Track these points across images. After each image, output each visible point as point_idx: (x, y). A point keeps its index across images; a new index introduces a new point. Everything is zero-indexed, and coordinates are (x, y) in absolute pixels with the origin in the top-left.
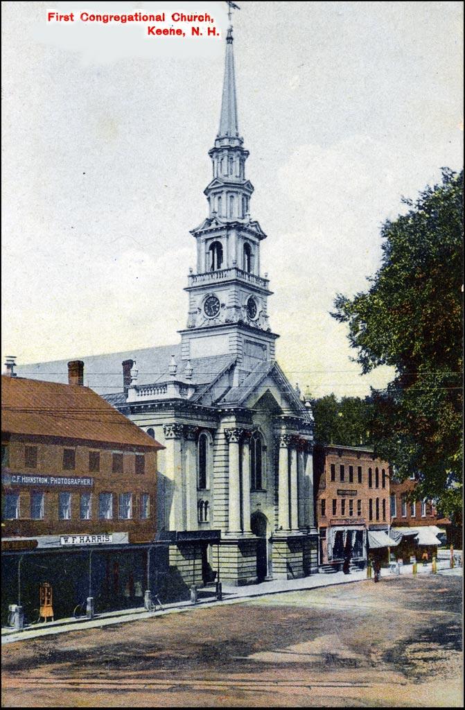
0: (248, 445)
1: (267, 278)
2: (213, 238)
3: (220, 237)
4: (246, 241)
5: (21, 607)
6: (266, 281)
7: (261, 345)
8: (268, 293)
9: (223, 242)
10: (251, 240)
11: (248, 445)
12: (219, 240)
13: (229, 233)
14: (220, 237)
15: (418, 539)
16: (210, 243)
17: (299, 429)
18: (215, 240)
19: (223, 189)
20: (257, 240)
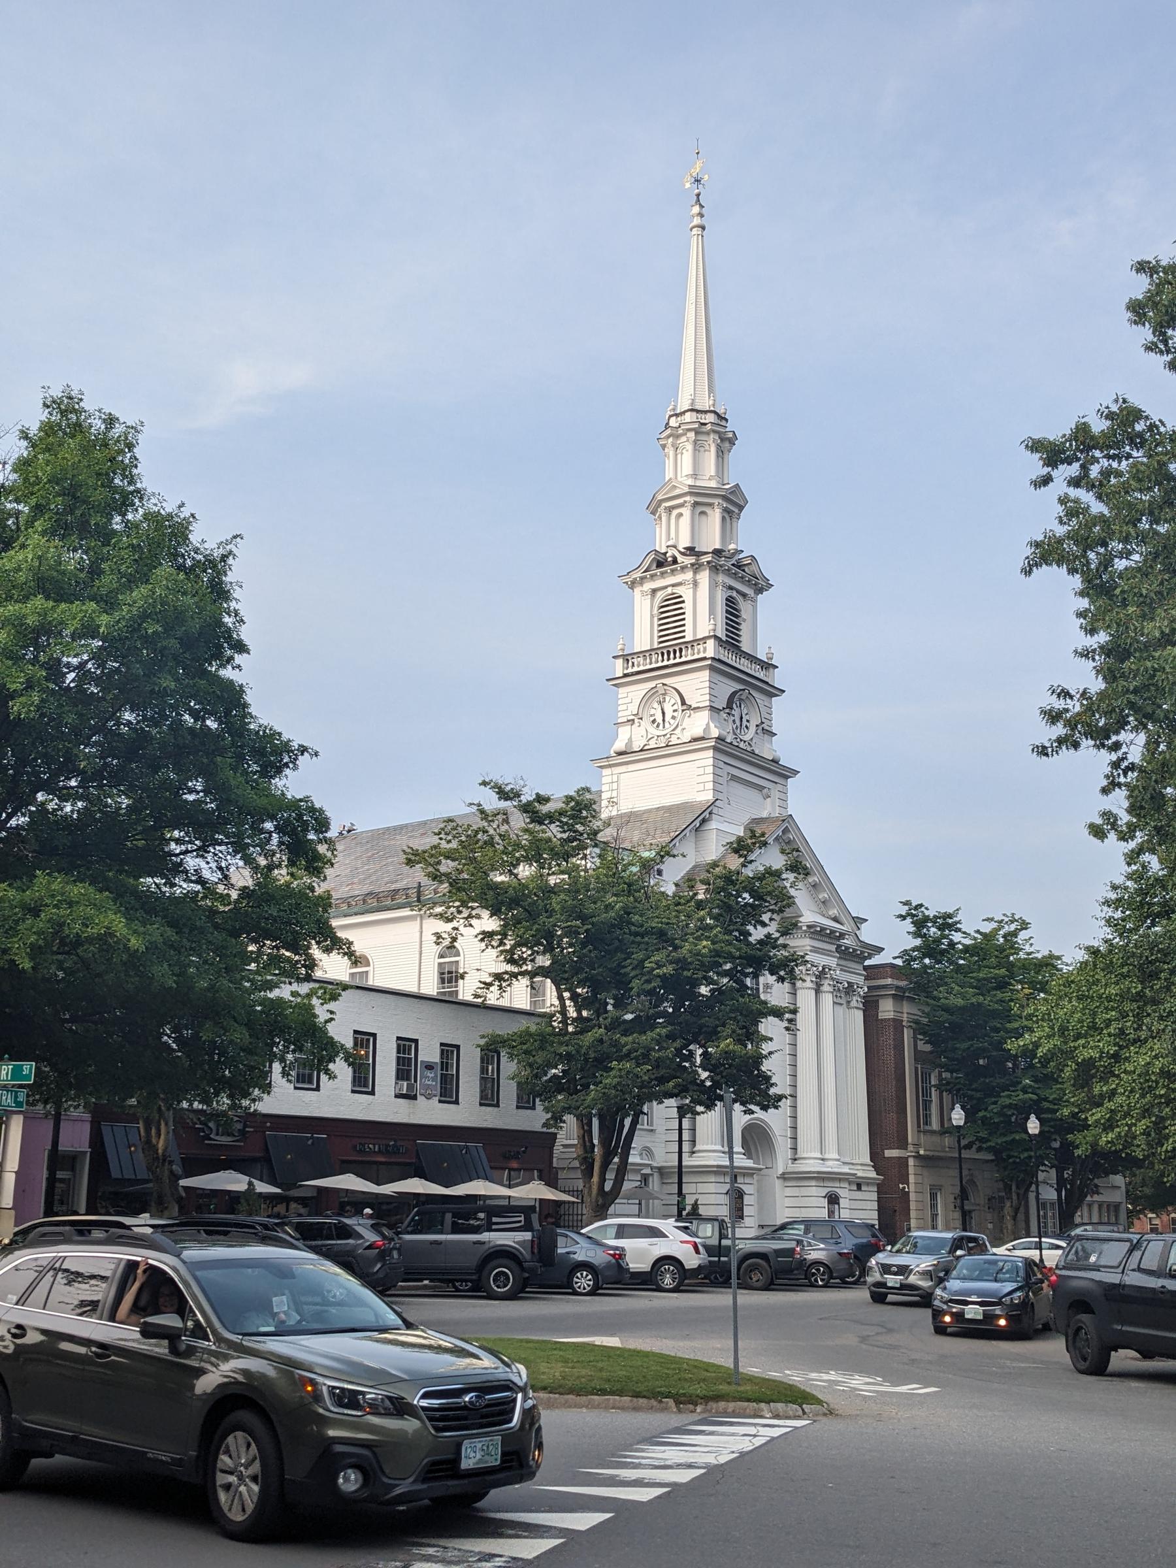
0: (21, 1117)
1: (773, 662)
2: (666, 587)
3: (679, 584)
4: (730, 593)
5: (1012, 1045)
6: (767, 666)
7: (760, 788)
8: (773, 692)
9: (686, 592)
10: (738, 592)
11: (21, 1117)
12: (679, 590)
13: (698, 577)
14: (679, 584)
15: (533, 1108)
16: (660, 595)
17: (135, 626)
18: (669, 590)
19: (688, 498)
20: (749, 591)
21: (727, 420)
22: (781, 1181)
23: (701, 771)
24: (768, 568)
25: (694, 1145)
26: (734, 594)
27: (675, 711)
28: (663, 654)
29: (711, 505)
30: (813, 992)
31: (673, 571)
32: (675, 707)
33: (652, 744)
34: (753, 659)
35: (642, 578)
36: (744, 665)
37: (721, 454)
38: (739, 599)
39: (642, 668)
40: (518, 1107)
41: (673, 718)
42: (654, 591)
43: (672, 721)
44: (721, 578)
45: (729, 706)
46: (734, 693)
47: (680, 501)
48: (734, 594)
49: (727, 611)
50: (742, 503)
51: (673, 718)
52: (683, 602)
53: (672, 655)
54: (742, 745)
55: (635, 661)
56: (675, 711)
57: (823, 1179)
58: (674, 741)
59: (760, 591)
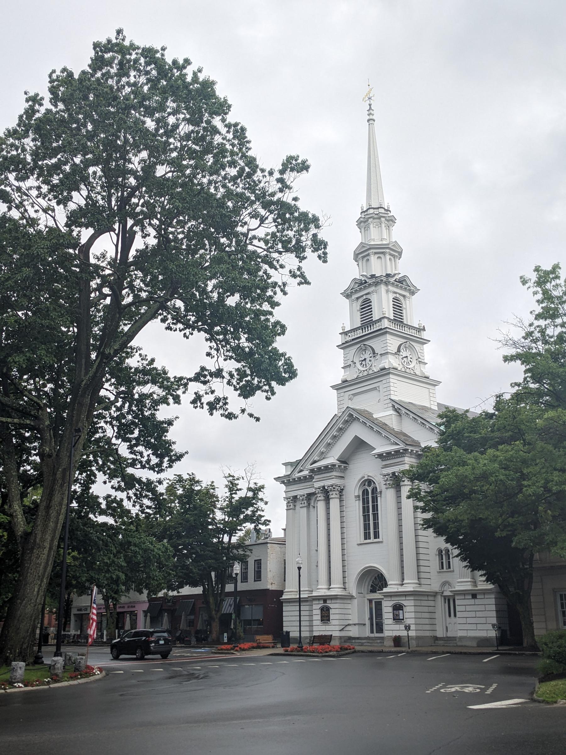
2: (362, 296)
10: (400, 294)
16: (361, 300)
18: (364, 297)
20: (407, 294)
21: (390, 211)
22: (353, 596)
23: (395, 385)
24: (414, 280)
25: (403, 579)
26: (398, 296)
27: (371, 357)
28: (362, 329)
29: (368, 255)
30: (338, 500)
31: (365, 287)
32: (371, 355)
33: (361, 375)
34: (411, 327)
35: (351, 293)
36: (407, 331)
37: (388, 227)
38: (401, 298)
39: (353, 337)
40: (261, 560)
41: (370, 361)
42: (358, 298)
43: (370, 363)
44: (391, 288)
45: (399, 350)
46: (401, 345)
47: (367, 253)
48: (398, 296)
49: (393, 305)
50: (400, 251)
51: (370, 361)
52: (371, 302)
53: (367, 329)
54: (408, 371)
55: (406, 329)
56: (371, 357)
57: (391, 596)
58: (371, 372)
59: (413, 293)
